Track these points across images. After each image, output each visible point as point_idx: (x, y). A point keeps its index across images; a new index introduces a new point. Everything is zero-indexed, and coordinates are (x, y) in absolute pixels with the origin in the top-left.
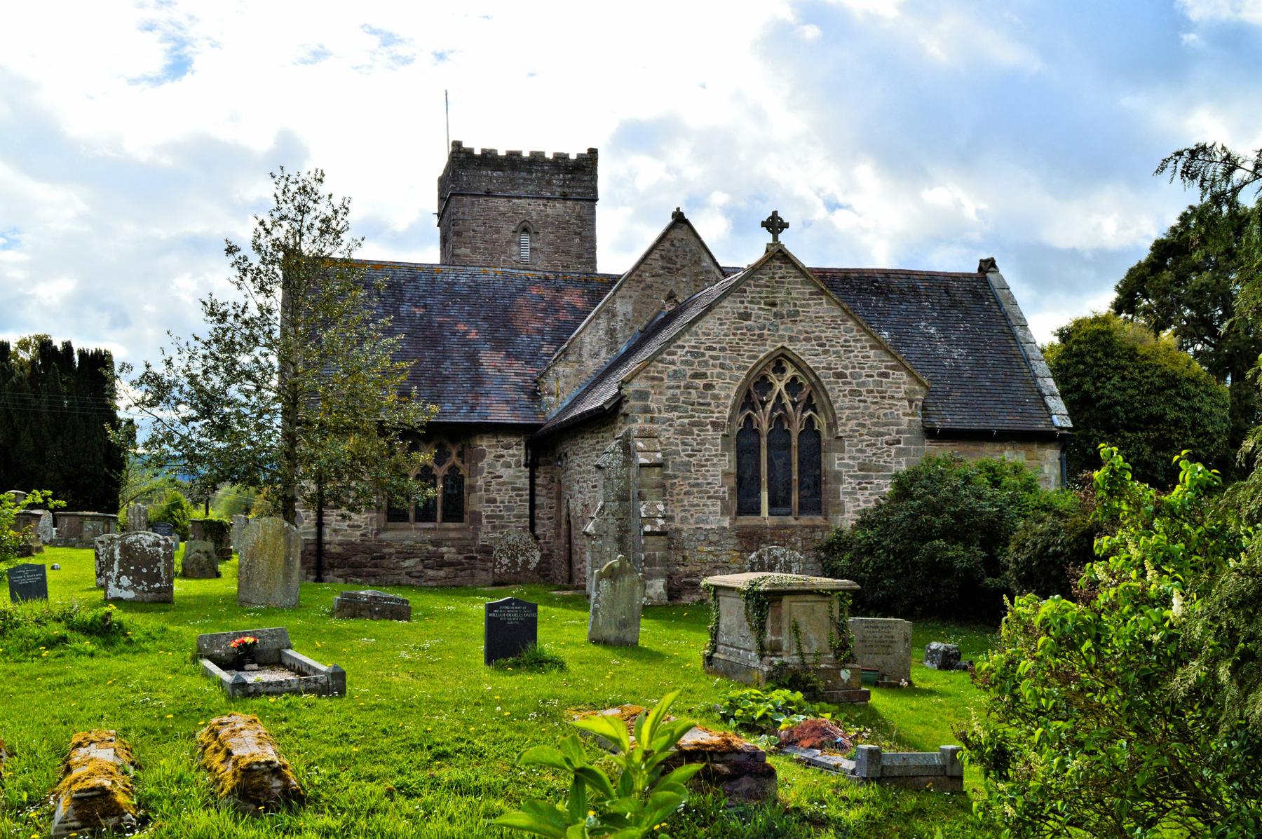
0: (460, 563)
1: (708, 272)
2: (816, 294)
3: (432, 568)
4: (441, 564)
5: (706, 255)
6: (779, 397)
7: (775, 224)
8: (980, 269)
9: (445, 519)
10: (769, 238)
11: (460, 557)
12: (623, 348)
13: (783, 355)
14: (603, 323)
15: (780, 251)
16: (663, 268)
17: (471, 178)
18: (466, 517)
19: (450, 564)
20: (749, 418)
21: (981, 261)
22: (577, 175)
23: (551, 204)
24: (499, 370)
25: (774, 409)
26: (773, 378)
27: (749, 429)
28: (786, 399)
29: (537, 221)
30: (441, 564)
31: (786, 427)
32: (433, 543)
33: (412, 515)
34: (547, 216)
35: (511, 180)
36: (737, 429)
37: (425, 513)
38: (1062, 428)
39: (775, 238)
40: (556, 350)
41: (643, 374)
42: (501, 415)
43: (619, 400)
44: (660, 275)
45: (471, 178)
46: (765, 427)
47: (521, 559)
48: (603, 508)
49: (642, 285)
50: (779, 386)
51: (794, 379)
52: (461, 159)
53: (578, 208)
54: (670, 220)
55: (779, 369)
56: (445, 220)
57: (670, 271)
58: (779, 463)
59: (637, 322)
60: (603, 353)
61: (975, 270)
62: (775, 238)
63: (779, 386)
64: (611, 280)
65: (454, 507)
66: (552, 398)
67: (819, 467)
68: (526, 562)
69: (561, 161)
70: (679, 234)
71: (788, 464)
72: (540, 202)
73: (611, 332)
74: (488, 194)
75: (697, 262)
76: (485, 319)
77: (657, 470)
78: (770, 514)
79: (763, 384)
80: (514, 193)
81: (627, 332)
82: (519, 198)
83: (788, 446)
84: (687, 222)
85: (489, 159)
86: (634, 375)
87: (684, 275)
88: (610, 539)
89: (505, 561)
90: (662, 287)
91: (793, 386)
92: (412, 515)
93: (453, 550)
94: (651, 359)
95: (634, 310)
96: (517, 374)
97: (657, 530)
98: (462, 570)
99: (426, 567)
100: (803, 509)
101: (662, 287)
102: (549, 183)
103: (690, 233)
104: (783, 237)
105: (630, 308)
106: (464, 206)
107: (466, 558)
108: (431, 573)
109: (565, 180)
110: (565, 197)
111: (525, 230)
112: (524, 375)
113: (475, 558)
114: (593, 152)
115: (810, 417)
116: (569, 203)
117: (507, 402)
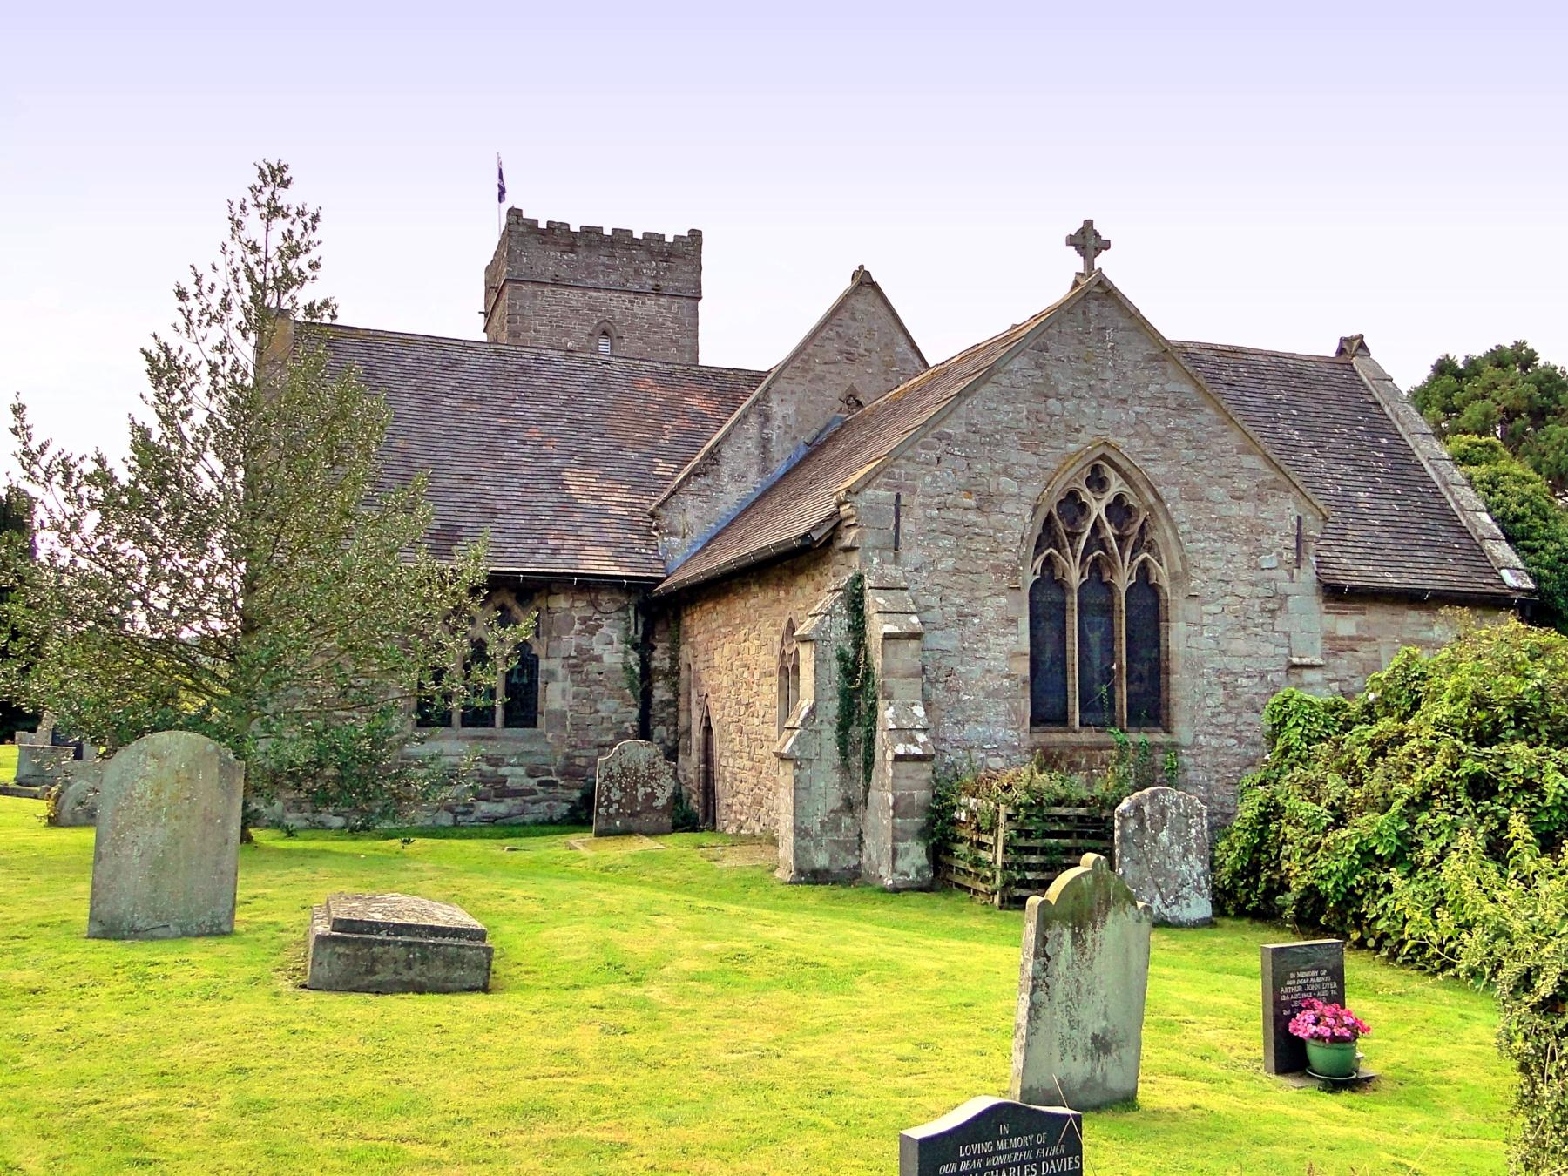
0: (532, 792)
1: (905, 361)
2: (1155, 358)
3: (486, 800)
4: (502, 791)
5: (901, 336)
6: (1096, 529)
7: (1087, 241)
8: (1341, 351)
9: (508, 723)
10: (1078, 263)
11: (532, 782)
12: (779, 468)
13: (1103, 457)
14: (752, 428)
15: (1100, 284)
16: (841, 352)
17: (534, 255)
18: (541, 720)
19: (516, 793)
20: (1049, 562)
21: (1343, 340)
22: (673, 264)
23: (639, 299)
24: (594, 498)
25: (1088, 550)
26: (1087, 496)
27: (1049, 579)
28: (1109, 531)
29: (619, 323)
30: (502, 791)
31: (1106, 577)
32: (489, 760)
33: (456, 718)
34: (634, 316)
35: (588, 266)
36: (1031, 579)
37: (477, 718)
38: (1519, 590)
39: (1090, 265)
40: (678, 471)
41: (881, 479)
42: (601, 564)
43: (836, 525)
44: (835, 363)
45: (534, 255)
46: (1075, 577)
47: (641, 791)
48: (812, 711)
49: (809, 377)
50: (1098, 508)
51: (1119, 498)
52: (519, 229)
53: (674, 307)
54: (847, 284)
55: (1097, 481)
56: (495, 321)
57: (850, 357)
58: (1095, 638)
59: (801, 431)
60: (753, 475)
61: (1331, 352)
62: (1090, 265)
63: (1098, 508)
64: (733, 386)
65: (522, 704)
66: (675, 540)
67: (1157, 645)
68: (651, 797)
69: (652, 242)
70: (860, 304)
71: (1109, 640)
72: (625, 297)
73: (764, 444)
74: (556, 282)
75: (889, 346)
76: (570, 422)
77: (913, 644)
78: (1081, 724)
79: (1072, 505)
80: (590, 283)
81: (787, 445)
82: (598, 289)
83: (1108, 610)
84: (874, 285)
85: (556, 234)
86: (868, 481)
87: (870, 365)
88: (825, 766)
89: (616, 794)
90: (838, 380)
91: (1119, 510)
92: (456, 718)
93: (521, 771)
94: (895, 455)
95: (798, 411)
96: (619, 504)
97: (917, 751)
98: (534, 803)
99: (478, 798)
100: (1135, 720)
101: (838, 380)
102: (637, 272)
103: (878, 301)
104: (1102, 261)
105: (791, 410)
106: (524, 296)
107: (540, 783)
108: (484, 807)
109: (657, 269)
110: (658, 292)
111: (605, 333)
112: (633, 505)
113: (554, 783)
114: (696, 236)
115: (1145, 561)
116: (664, 300)
117: (607, 544)
